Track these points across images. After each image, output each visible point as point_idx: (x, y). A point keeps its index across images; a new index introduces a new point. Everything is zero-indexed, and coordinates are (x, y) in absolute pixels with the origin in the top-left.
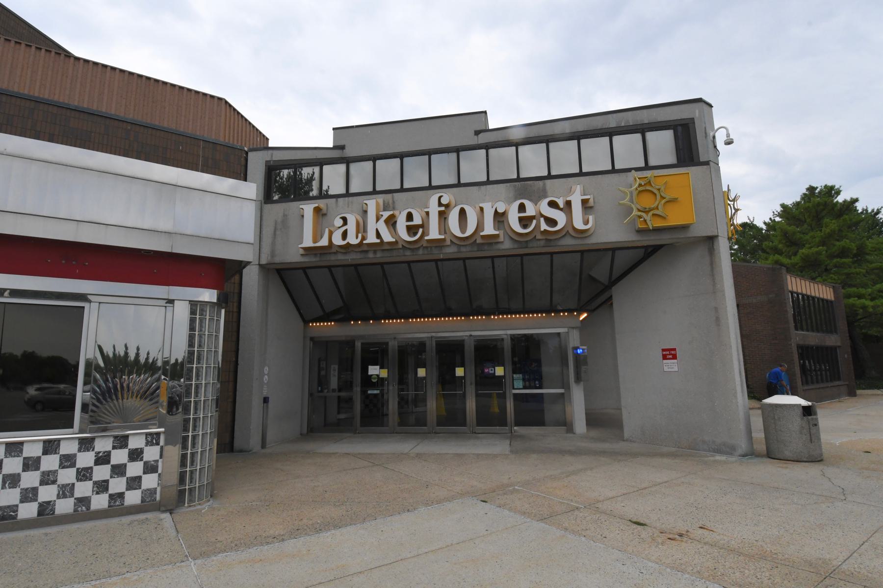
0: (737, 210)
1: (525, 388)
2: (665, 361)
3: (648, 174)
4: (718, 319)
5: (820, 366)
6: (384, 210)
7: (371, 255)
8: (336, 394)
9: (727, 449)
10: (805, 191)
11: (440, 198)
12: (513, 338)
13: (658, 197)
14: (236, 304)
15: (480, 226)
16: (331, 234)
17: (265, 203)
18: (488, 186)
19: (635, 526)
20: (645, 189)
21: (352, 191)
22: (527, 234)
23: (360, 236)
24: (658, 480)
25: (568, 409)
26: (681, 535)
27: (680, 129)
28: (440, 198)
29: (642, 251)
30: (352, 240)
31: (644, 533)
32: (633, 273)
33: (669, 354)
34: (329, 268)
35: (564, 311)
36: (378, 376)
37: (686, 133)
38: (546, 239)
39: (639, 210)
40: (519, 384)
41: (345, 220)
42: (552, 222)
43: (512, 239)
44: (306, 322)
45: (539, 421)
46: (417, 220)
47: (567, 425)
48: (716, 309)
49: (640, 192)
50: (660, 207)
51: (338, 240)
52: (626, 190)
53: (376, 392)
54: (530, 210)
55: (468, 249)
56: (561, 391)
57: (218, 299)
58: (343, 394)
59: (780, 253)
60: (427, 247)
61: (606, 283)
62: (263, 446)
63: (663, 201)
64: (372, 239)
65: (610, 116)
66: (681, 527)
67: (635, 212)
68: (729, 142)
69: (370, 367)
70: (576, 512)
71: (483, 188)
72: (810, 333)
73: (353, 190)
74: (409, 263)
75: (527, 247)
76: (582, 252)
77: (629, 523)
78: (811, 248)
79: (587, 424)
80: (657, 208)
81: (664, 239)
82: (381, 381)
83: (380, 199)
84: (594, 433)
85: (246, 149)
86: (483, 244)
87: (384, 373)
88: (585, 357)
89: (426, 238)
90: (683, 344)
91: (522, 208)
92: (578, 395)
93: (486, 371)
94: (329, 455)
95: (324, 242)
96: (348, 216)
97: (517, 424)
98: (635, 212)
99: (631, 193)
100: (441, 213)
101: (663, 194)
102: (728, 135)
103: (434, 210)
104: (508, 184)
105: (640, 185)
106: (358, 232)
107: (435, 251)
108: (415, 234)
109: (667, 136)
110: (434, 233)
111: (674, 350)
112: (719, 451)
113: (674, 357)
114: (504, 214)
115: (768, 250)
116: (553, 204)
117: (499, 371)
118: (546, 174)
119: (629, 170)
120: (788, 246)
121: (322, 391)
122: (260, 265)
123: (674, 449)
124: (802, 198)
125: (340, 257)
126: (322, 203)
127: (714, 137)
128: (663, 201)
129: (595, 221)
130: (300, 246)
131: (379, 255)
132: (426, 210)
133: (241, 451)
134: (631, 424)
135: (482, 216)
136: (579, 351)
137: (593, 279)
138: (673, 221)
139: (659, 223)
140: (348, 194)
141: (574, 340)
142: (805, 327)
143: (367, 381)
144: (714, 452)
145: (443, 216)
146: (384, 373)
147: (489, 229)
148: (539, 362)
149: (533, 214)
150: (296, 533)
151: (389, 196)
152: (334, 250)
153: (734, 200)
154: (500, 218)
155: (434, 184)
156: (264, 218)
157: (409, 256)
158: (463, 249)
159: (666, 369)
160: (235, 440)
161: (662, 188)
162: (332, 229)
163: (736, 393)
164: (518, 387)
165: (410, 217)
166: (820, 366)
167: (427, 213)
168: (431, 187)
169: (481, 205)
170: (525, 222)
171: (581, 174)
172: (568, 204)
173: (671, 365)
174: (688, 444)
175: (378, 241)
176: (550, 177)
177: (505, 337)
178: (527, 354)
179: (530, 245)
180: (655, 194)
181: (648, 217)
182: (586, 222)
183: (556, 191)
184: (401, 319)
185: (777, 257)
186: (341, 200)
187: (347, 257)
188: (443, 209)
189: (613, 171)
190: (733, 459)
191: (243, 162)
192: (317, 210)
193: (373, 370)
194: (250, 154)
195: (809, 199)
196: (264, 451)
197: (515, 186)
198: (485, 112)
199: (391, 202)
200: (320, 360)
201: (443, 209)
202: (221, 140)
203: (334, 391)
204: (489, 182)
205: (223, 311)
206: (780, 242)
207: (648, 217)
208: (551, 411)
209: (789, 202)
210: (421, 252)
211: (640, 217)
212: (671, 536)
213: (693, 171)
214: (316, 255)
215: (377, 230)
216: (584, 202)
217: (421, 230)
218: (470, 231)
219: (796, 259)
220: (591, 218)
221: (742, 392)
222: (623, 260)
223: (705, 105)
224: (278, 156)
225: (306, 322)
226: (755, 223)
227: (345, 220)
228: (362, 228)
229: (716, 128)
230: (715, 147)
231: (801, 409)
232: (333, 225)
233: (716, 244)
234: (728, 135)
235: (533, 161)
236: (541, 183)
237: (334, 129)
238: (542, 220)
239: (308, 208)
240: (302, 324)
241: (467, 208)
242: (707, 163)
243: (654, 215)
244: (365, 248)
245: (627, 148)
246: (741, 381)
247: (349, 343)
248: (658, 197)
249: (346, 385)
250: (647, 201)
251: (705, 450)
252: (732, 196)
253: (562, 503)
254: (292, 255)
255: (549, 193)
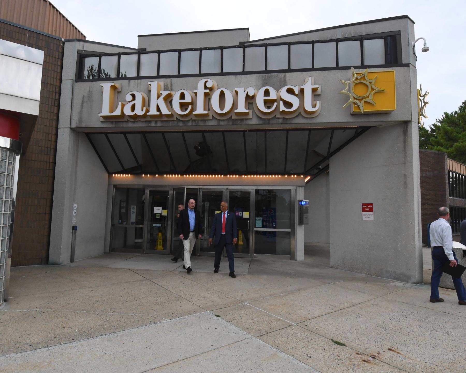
0: (425, 103)
1: (263, 227)
2: (364, 213)
3: (363, 71)
4: (405, 183)
5: (456, 221)
6: (165, 90)
7: (153, 124)
8: (135, 226)
9: (404, 278)
10: (461, 104)
11: (206, 82)
12: (257, 191)
13: (370, 89)
14: (52, 157)
15: (235, 106)
16: (123, 106)
17: (76, 81)
18: (243, 76)
19: (336, 346)
20: (360, 82)
21: (142, 74)
22: (269, 113)
23: (145, 109)
24: (355, 302)
25: (292, 242)
26: (373, 357)
27: (389, 38)
28: (206, 82)
29: (354, 131)
30: (139, 111)
31: (344, 353)
32: (346, 147)
33: (367, 207)
34: (125, 133)
35: (294, 174)
36: (160, 214)
37: (393, 43)
38: (284, 118)
39: (355, 98)
40: (259, 224)
41: (134, 96)
42: (288, 104)
43: (258, 117)
44: (110, 174)
45: (272, 251)
46: (188, 99)
47: (291, 254)
48: (405, 176)
49: (356, 84)
50: (370, 96)
51: (128, 112)
52: (346, 82)
53: (158, 225)
54: (273, 95)
55: (226, 123)
56: (289, 230)
57: (11, 146)
58: (138, 226)
59: (442, 146)
60: (195, 120)
61: (326, 155)
62: (72, 260)
63: (374, 92)
64: (153, 111)
65: (337, 29)
66: (374, 350)
67: (351, 100)
68: (425, 50)
69: (155, 208)
70: (289, 330)
71: (239, 77)
72: (458, 199)
73: (142, 74)
74: (183, 132)
75: (269, 124)
76: (310, 130)
77: (331, 343)
78: (462, 142)
79: (305, 254)
80: (368, 97)
81: (372, 121)
82: (162, 217)
83: (162, 82)
84: (310, 260)
85: (63, 40)
86: (236, 119)
87: (165, 213)
88: (307, 208)
89: (194, 113)
90: (377, 200)
91: (267, 93)
92: (300, 232)
93: (237, 214)
94: (116, 269)
95: (117, 113)
96: (136, 93)
97: (256, 252)
98: (351, 100)
99: (350, 84)
100: (206, 95)
101: (374, 87)
102: (425, 44)
103: (201, 91)
104: (258, 75)
105: (357, 79)
106: (143, 105)
107: (201, 124)
108: (186, 109)
109: (380, 43)
110: (200, 110)
111: (372, 204)
112: (398, 279)
113: (371, 210)
114: (253, 97)
115: (433, 143)
116: (290, 91)
117: (246, 215)
118: (287, 68)
119: (349, 68)
120: (446, 141)
121: (122, 223)
122: (71, 129)
123: (364, 276)
124: (460, 109)
125: (131, 125)
126: (117, 83)
127: (414, 46)
128: (374, 92)
129: (321, 105)
130: (100, 115)
131: (159, 124)
132: (195, 91)
133: (54, 264)
134: (336, 256)
135: (237, 96)
136: (303, 203)
137: (316, 154)
138: (379, 108)
139: (369, 109)
140: (139, 77)
141: (300, 194)
142: (455, 194)
143: (154, 218)
144: (394, 279)
145: (207, 96)
146: (165, 213)
147: (241, 108)
148: (275, 210)
149: (275, 97)
150: (54, 340)
151: (168, 80)
152: (125, 119)
153: (424, 96)
154: (250, 99)
155: (203, 72)
156: (75, 93)
157: (181, 127)
158: (222, 123)
159: (364, 218)
160: (50, 256)
161: (373, 82)
162: (124, 103)
163: (414, 237)
164: (259, 226)
165: (182, 96)
166: (456, 221)
167: (196, 94)
168: (200, 75)
169: (236, 89)
170: (268, 103)
171: (313, 69)
172: (302, 91)
173: (368, 216)
174: (374, 272)
175: (158, 113)
176: (290, 70)
177: (251, 191)
178: (267, 203)
179: (272, 122)
180: (367, 87)
181: (361, 104)
182: (314, 106)
183: (293, 80)
184: (178, 174)
185: (439, 147)
186: (132, 82)
187: (136, 125)
188: (207, 91)
189: (338, 68)
190: (408, 285)
191: (60, 50)
192: (114, 88)
193: (158, 210)
194: (66, 43)
195: (464, 110)
196: (72, 264)
197: (263, 77)
198: (248, 29)
199: (169, 84)
200: (121, 201)
201: (207, 91)
202: (45, 32)
203: (133, 223)
204: (244, 73)
205: (18, 158)
206: (442, 138)
207: (361, 104)
208: (281, 244)
209: (449, 113)
210: (190, 124)
211: (355, 103)
212: (365, 358)
213: (397, 70)
214: (112, 122)
215: (158, 105)
216: (314, 90)
217: (190, 107)
218: (227, 108)
219: (450, 150)
220: (318, 103)
221: (419, 237)
222: (339, 137)
223: (409, 20)
224: (88, 48)
225: (110, 174)
226: (424, 126)
227: (134, 96)
228: (146, 103)
229: (416, 39)
230: (414, 53)
231: (462, 251)
232: (126, 101)
233: (409, 127)
234: (425, 44)
235: (278, 59)
236: (282, 75)
237: (139, 36)
238: (281, 103)
239: (107, 86)
240: (107, 175)
241: (226, 91)
242: (408, 65)
243: (365, 102)
244: (149, 119)
245: (349, 52)
246: (419, 230)
247: (141, 191)
248: (370, 89)
249: (140, 220)
250: (361, 91)
251: (387, 277)
252: (423, 93)
253: (279, 320)
254: (95, 122)
255: (288, 82)
